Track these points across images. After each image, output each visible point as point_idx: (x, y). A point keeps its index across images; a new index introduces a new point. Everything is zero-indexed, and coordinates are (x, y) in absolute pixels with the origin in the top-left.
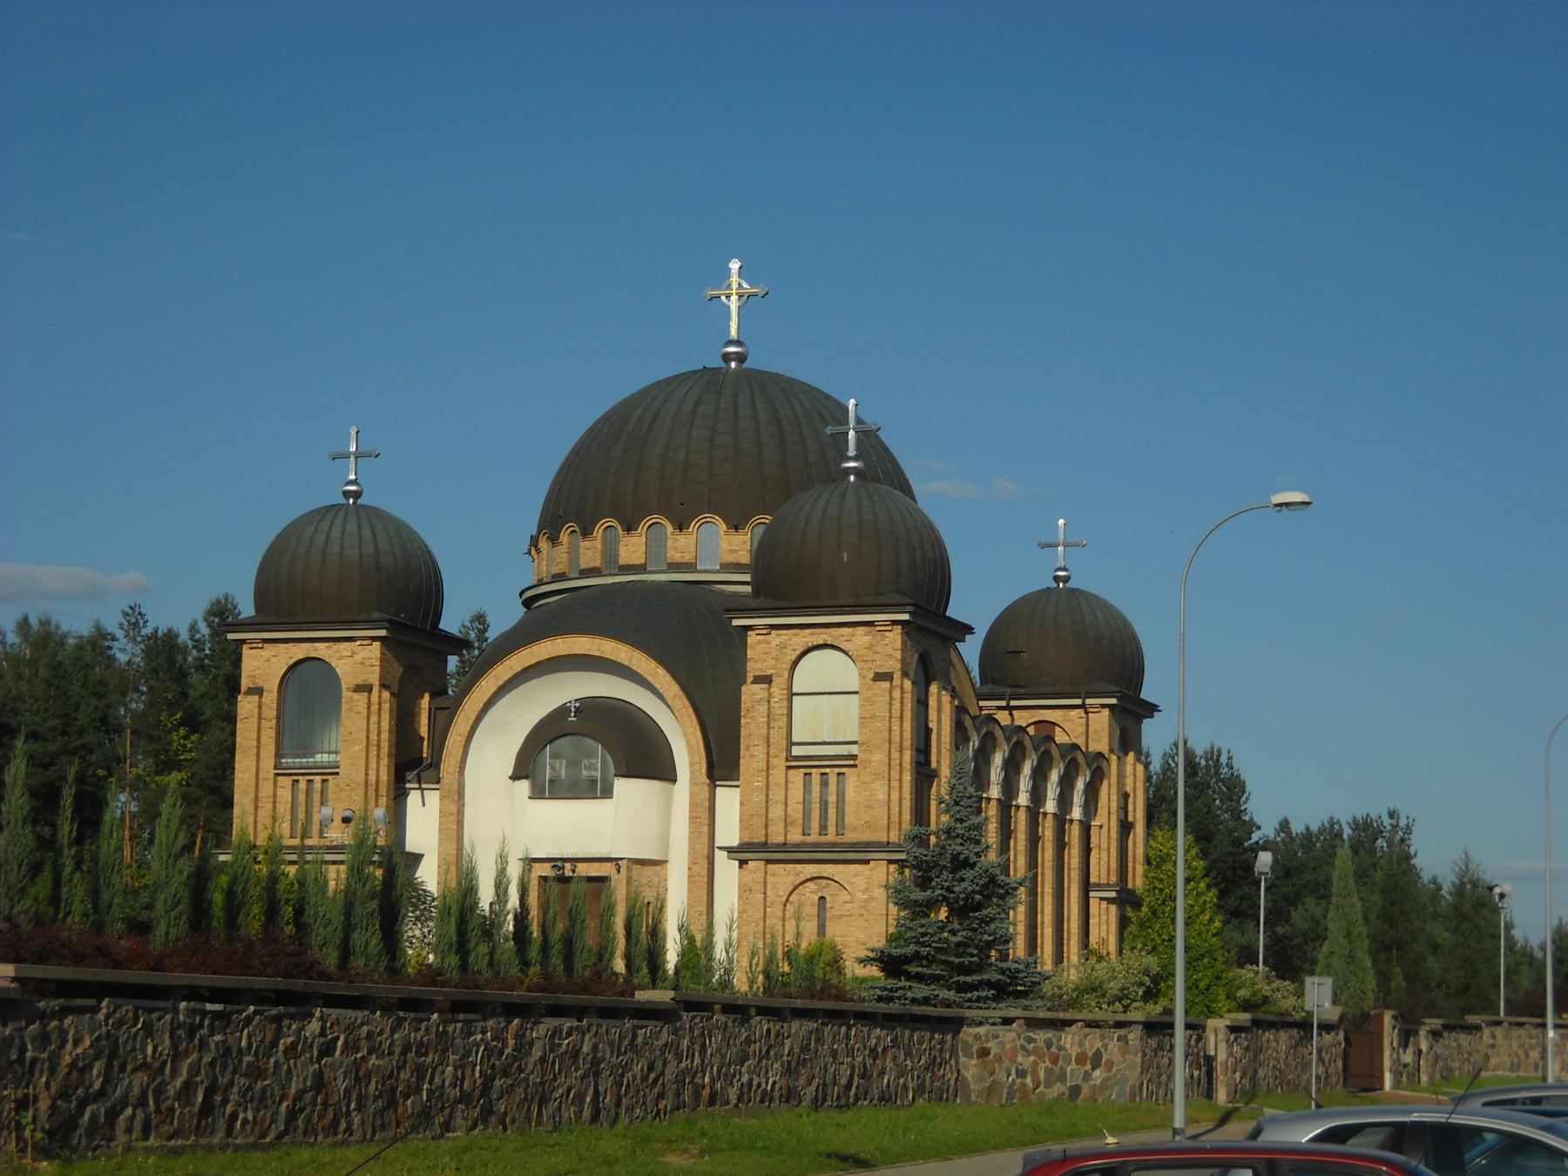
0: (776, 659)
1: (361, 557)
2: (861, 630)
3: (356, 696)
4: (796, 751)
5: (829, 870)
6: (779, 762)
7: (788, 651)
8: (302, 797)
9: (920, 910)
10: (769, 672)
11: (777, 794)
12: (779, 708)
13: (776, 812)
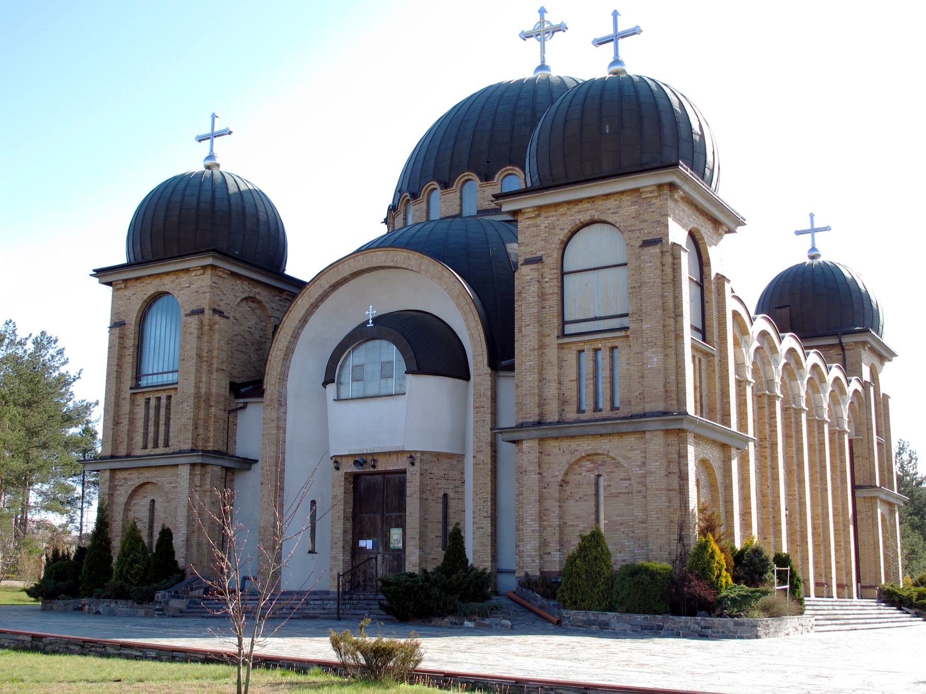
0: (545, 240)
1: (199, 202)
2: (627, 199)
3: (190, 319)
4: (570, 329)
5: (604, 445)
6: (552, 341)
7: (557, 231)
8: (152, 412)
9: (60, 527)
10: (539, 254)
11: (552, 373)
12: (552, 287)
13: (551, 391)
